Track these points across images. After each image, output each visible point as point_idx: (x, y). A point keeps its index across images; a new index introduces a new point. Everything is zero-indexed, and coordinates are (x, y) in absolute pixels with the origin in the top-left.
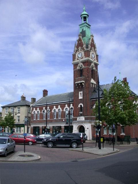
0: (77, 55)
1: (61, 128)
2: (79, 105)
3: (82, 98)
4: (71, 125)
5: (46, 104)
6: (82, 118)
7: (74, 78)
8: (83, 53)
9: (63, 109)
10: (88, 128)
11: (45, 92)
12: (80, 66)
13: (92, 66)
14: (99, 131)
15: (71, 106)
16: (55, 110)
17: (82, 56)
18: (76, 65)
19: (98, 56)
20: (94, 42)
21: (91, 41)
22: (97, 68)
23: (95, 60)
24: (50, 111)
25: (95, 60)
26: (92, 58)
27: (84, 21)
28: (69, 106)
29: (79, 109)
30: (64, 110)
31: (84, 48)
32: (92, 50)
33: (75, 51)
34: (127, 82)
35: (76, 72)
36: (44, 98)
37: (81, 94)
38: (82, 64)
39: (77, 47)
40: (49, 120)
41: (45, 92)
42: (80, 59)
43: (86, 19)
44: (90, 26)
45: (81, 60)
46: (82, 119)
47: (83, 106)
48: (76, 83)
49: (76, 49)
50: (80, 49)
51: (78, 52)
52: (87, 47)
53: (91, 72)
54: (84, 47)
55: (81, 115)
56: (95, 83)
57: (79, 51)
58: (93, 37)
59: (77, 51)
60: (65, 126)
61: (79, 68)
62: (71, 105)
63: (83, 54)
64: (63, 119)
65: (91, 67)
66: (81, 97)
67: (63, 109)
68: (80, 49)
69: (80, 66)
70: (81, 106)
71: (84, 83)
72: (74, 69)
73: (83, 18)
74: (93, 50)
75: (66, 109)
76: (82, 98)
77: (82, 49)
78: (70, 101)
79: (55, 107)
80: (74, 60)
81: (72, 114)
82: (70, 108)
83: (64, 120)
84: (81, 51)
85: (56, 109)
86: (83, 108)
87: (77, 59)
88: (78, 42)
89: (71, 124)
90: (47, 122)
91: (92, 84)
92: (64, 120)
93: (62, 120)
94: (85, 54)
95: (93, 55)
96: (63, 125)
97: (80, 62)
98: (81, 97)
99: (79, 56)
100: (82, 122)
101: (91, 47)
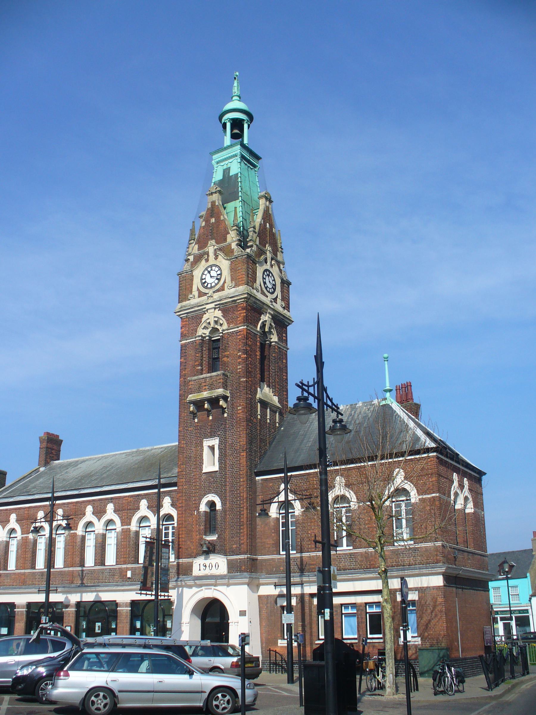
0: (197, 273)
1: (116, 611)
2: (205, 500)
3: (216, 468)
4: (162, 596)
5: (50, 495)
6: (219, 564)
7: (183, 376)
8: (225, 264)
9: (126, 521)
10: (243, 613)
11: (52, 447)
12: (212, 324)
13: (263, 325)
14: (327, 617)
15: (167, 508)
16: (89, 524)
17: (219, 280)
18: (192, 320)
19: (289, 284)
20: (271, 226)
21: (258, 219)
22: (283, 338)
23: (275, 300)
24: (68, 527)
25: (275, 300)
26: (263, 293)
27: (234, 136)
28: (156, 507)
29: (203, 518)
30: (134, 526)
31: (230, 245)
32: (263, 257)
33: (191, 258)
34: (416, 401)
35: (191, 352)
36: (42, 469)
37: (212, 448)
38: (219, 313)
39: (198, 242)
40: (61, 573)
41: (52, 447)
42: (210, 292)
43: (242, 130)
44: (258, 158)
45: (216, 296)
46: (217, 566)
47: (219, 506)
48: (191, 397)
49: (195, 249)
50: (211, 250)
51: (203, 264)
52: (243, 243)
53: (258, 353)
54: (229, 239)
55: (210, 550)
56: (275, 400)
57: (207, 260)
58: (271, 202)
59: (198, 259)
60: (134, 603)
61: (207, 332)
62: (167, 501)
63: (226, 274)
64: (128, 569)
65: (258, 329)
66: (210, 464)
67: (126, 521)
68: (211, 250)
69: (212, 324)
70: (212, 505)
71: (225, 398)
72: (183, 336)
73: (228, 126)
74: (269, 255)
75: (144, 518)
76: (216, 468)
77: (220, 249)
78: (163, 481)
79: (89, 509)
80: (183, 296)
81: (167, 541)
82: (162, 513)
83: (129, 574)
84: (216, 258)
85: (94, 519)
86: (219, 518)
87: (196, 293)
88: (207, 221)
89: (166, 589)
90: (48, 582)
91: (265, 404)
92: (129, 574)
93: (122, 573)
94: (233, 270)
95: (267, 281)
96: (124, 596)
97: (213, 305)
98: (210, 464)
99: (209, 280)
100: (214, 580)
101: (263, 243)
